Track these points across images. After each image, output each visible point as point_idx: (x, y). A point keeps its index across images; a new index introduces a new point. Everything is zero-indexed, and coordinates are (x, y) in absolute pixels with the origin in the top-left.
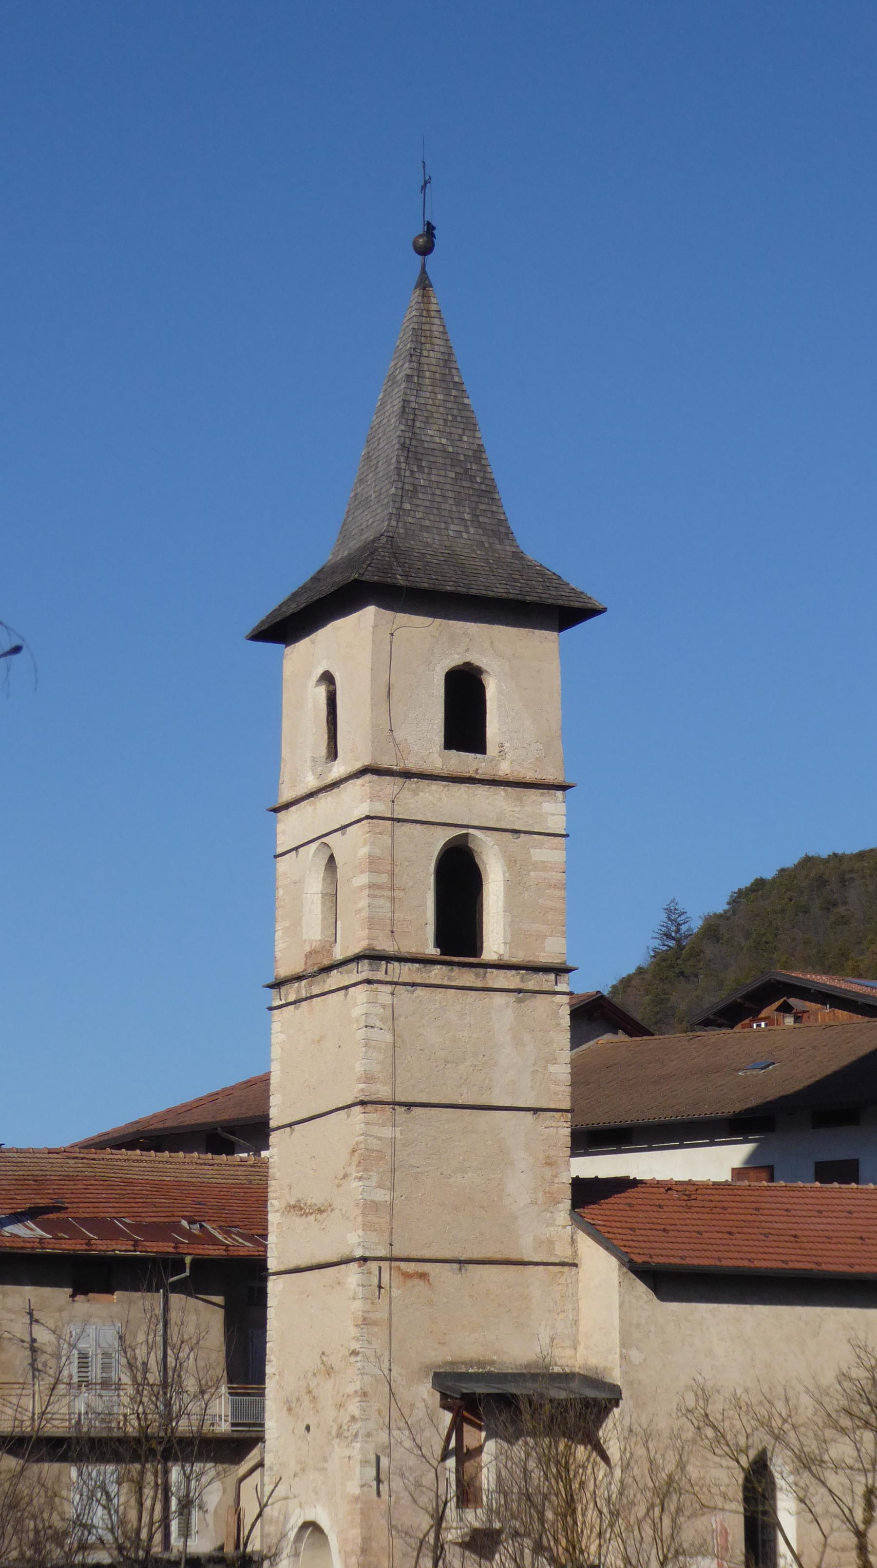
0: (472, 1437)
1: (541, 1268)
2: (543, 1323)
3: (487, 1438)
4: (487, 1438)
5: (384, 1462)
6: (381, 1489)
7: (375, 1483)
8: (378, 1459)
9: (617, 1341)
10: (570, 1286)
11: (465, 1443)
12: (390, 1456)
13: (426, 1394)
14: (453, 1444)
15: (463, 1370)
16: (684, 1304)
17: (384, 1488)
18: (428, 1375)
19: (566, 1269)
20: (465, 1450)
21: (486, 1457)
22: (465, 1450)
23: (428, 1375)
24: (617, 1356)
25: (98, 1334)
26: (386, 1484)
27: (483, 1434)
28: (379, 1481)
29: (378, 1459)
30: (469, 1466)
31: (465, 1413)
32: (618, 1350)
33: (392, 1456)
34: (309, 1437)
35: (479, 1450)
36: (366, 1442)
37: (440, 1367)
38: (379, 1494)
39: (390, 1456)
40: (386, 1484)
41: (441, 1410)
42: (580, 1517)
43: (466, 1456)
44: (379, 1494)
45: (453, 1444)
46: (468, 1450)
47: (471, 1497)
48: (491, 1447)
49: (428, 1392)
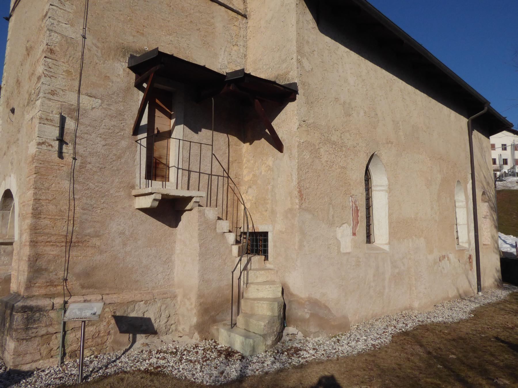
0: (162, 123)
1: (223, 8)
2: (223, 49)
3: (176, 124)
4: (176, 124)
5: (70, 124)
6: (64, 150)
7: (56, 144)
8: (63, 120)
9: (294, 48)
10: (242, 29)
11: (156, 126)
12: (77, 120)
13: (122, 74)
14: (144, 121)
15: (91, 290)
16: (333, 41)
17: (68, 150)
18: (124, 55)
19: (240, 17)
20: (156, 132)
21: (173, 144)
22: (156, 132)
23: (124, 55)
24: (294, 60)
25: (247, 323)
26: (71, 146)
27: (173, 121)
28: (61, 141)
29: (63, 120)
30: (159, 145)
31: (157, 101)
32: (295, 56)
33: (81, 121)
34: (13, 117)
35: (168, 135)
36: (50, 99)
37: (137, 52)
38: (61, 155)
39: (77, 120)
40: (71, 146)
41: (136, 89)
42: (294, 179)
43: (156, 137)
44: (61, 155)
45: (144, 121)
46: (158, 131)
47: (159, 172)
48: (180, 131)
49: (124, 70)
